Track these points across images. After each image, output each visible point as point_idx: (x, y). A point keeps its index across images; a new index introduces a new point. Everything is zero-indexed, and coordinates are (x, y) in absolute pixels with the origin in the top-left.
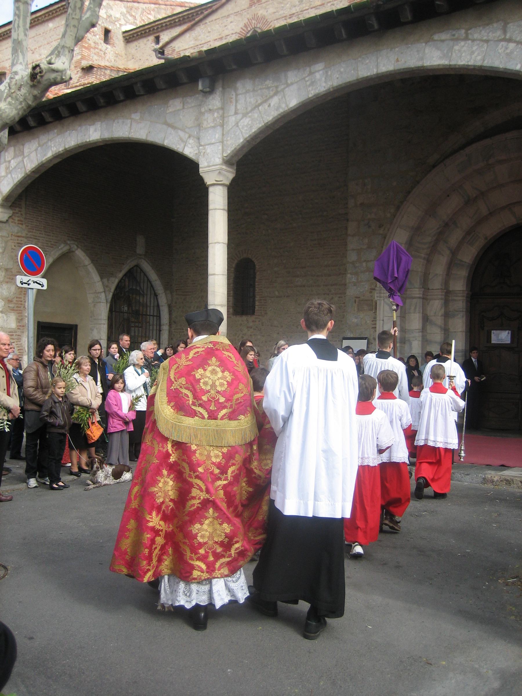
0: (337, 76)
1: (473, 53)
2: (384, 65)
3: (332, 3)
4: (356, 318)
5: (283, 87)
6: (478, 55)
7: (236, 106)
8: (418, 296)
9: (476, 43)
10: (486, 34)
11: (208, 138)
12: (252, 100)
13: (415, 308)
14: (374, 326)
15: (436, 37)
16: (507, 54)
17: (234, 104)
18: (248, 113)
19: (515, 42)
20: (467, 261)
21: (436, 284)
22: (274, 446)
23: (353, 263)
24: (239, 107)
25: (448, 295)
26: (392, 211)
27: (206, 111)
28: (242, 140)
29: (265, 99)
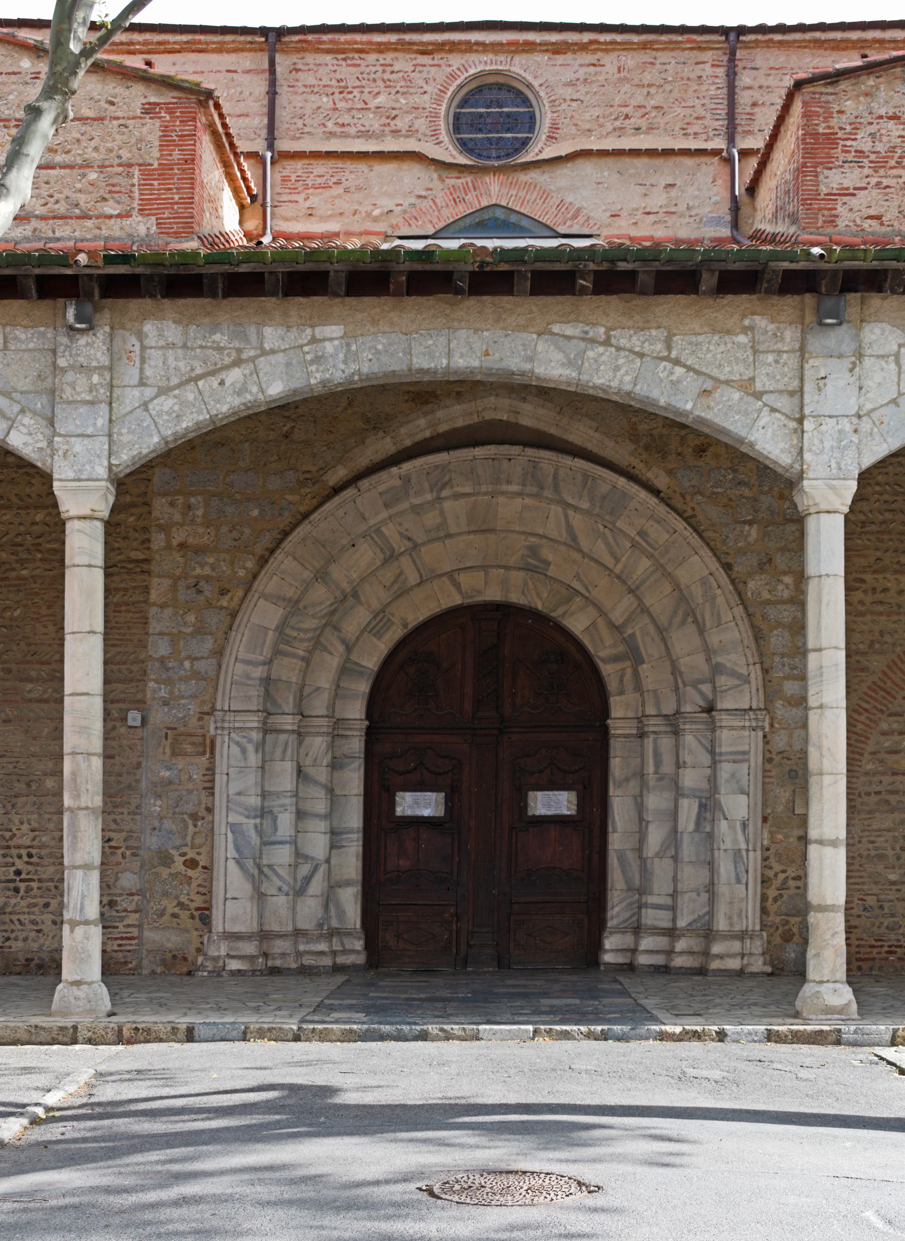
0: (370, 357)
1: (617, 368)
2: (462, 356)
3: (121, 121)
4: (168, 768)
5: (252, 353)
6: (627, 373)
7: (142, 370)
8: (289, 727)
9: (622, 353)
10: (639, 343)
11: (78, 422)
12: (181, 364)
13: (284, 752)
14: (208, 785)
15: (556, 328)
17: (138, 364)
18: (171, 389)
19: (684, 366)
20: (370, 666)
23: (162, 660)
24: (148, 372)
25: (337, 729)
26: (249, 565)
27: (72, 367)
29: (212, 368)
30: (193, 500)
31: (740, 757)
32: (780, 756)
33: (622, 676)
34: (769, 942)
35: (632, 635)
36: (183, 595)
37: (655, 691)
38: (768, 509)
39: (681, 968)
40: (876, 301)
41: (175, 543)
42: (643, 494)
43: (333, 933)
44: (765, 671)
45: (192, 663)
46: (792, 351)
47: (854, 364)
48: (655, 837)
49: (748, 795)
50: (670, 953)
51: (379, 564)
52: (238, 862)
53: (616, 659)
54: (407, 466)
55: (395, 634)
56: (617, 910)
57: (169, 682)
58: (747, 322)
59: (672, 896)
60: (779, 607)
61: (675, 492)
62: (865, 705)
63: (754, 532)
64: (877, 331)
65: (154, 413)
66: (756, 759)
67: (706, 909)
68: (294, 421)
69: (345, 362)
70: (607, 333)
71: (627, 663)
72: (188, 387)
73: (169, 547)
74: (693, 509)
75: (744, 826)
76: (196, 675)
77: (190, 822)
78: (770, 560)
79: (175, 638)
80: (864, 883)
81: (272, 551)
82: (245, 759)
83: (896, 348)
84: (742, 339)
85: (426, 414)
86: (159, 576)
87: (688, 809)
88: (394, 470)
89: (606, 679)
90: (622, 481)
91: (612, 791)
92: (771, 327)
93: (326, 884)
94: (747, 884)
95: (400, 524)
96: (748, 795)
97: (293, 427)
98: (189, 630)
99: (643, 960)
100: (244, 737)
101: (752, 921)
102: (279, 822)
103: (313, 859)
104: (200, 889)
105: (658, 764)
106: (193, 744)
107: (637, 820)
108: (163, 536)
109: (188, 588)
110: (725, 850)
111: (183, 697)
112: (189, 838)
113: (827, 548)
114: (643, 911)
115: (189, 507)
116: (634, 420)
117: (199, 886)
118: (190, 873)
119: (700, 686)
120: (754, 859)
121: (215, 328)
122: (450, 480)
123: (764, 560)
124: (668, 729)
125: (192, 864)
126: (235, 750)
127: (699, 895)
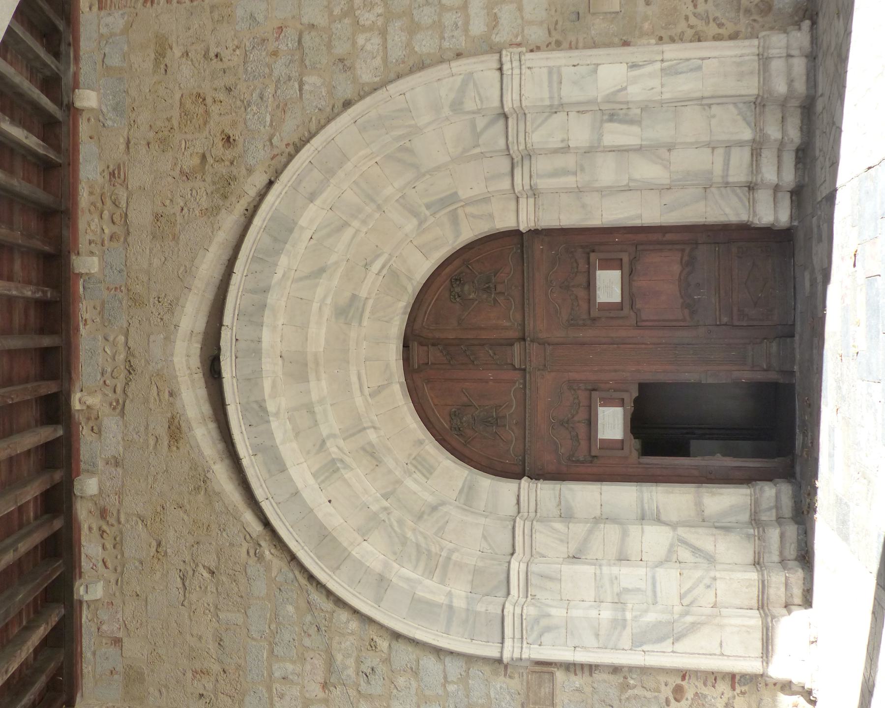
30: (277, 674)
31: (555, 77)
32: (553, 33)
33: (474, 216)
34: (772, 29)
35: (428, 206)
36: (377, 687)
38: (287, 66)
39: (801, 129)
41: (321, 695)
42: (270, 198)
43: (755, 521)
44: (459, 55)
45: (449, 683)
48: (647, 170)
49: (598, 65)
52: (677, 639)
53: (454, 219)
54: (243, 450)
59: (713, 148)
60: (389, 46)
61: (269, 166)
63: (311, 80)
66: (558, 58)
67: (731, 107)
68: (197, 565)
71: (460, 212)
74: (287, 145)
75: (633, 66)
77: (630, 692)
78: (341, 60)
85: (190, 429)
87: (617, 135)
90: (257, 221)
93: (700, 530)
94: (703, 59)
96: (598, 65)
97: (204, 567)
98: (414, 684)
99: (789, 177)
100: (532, 628)
101: (746, 49)
102: (630, 587)
103: (672, 545)
109: (368, 682)
110: (662, 86)
111: (488, 695)
112: (648, 694)
116: (197, 212)
117: (705, 684)
118: (690, 694)
119: (478, 130)
120: (672, 52)
123: (341, 66)
124: (526, 163)
127: (714, 116)
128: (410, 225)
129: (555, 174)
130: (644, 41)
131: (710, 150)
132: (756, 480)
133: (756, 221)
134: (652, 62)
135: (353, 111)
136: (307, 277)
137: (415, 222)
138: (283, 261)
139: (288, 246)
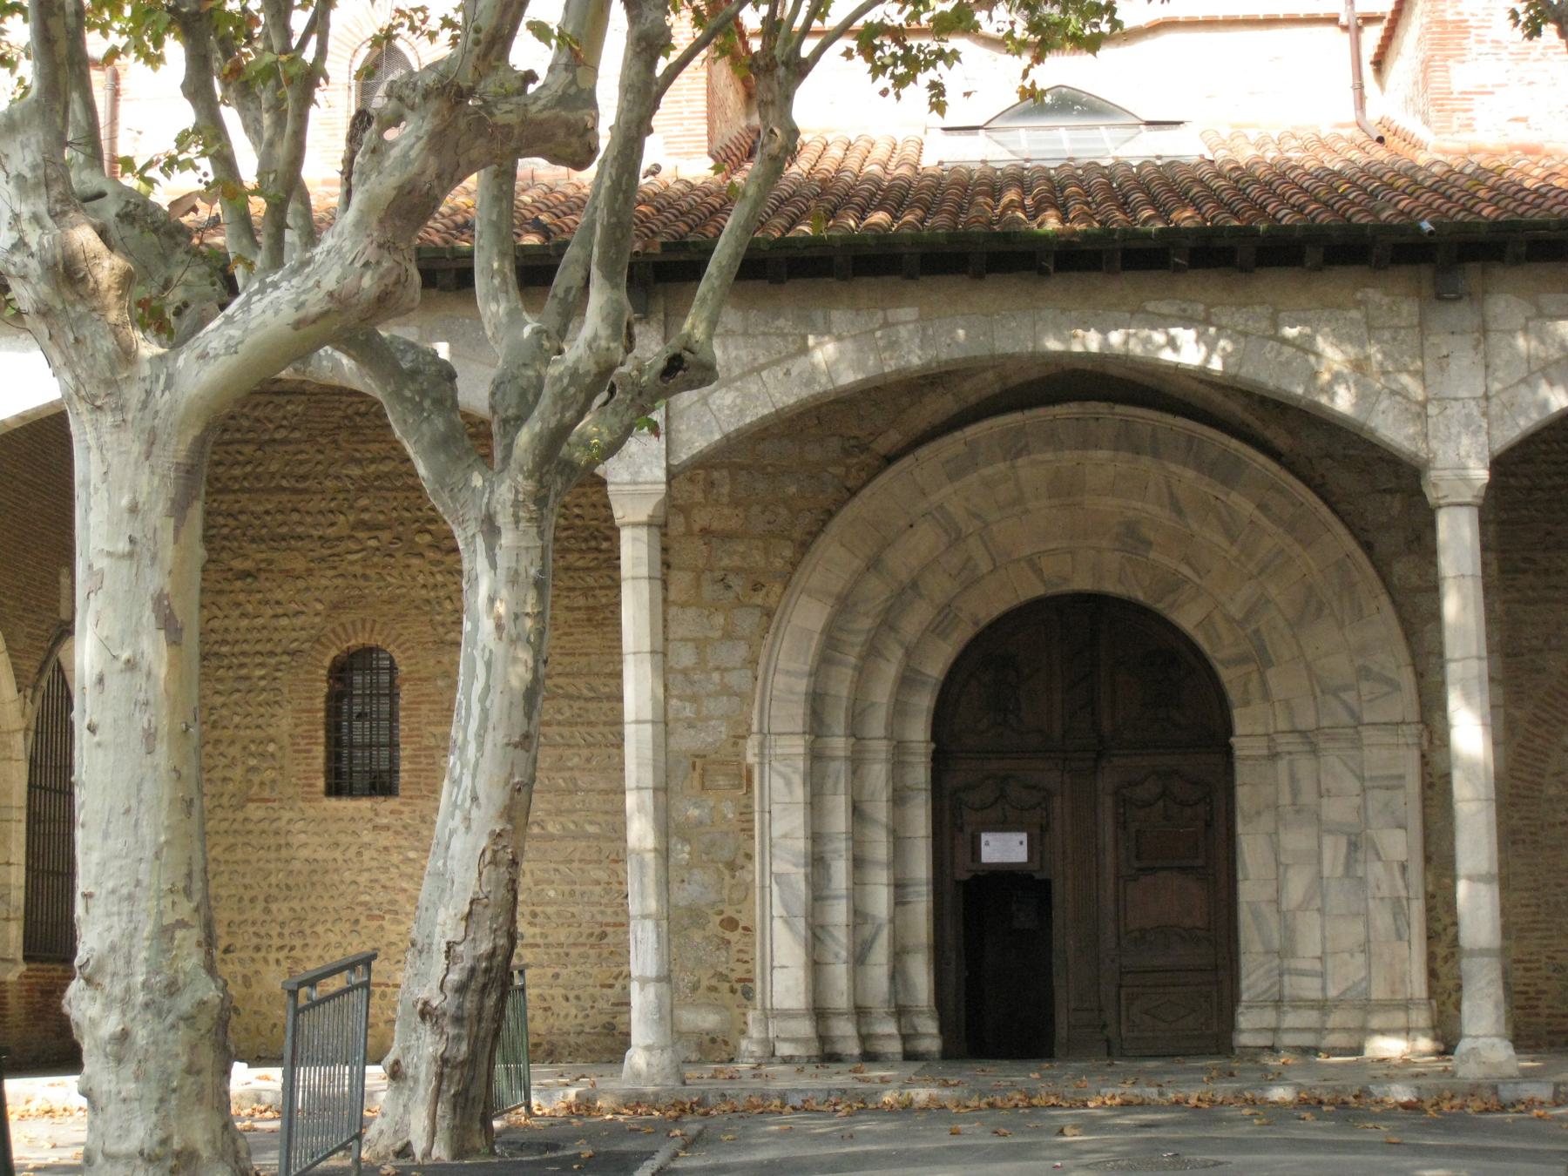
14: (745, 825)
15: (1151, 306)
16: (1280, 363)
21: (877, 725)
22: (1507, 987)
23: (685, 672)
26: (788, 553)
28: (717, 437)
30: (716, 475)
35: (1257, 631)
36: (708, 591)
37: (1287, 702)
40: (1498, 271)
41: (696, 528)
42: (1262, 459)
46: (1412, 327)
47: (1478, 340)
50: (1321, 1031)
51: (943, 548)
52: (786, 922)
53: (1242, 659)
54: (971, 431)
55: (962, 634)
56: (1254, 977)
57: (694, 699)
58: (1359, 295)
59: (1320, 958)
62: (1543, 715)
64: (1502, 304)
65: (714, 407)
67: (1363, 974)
69: (921, 348)
70: (1207, 311)
71: (1252, 667)
72: (751, 379)
73: (689, 533)
74: (1323, 476)
75: (1404, 868)
76: (727, 690)
77: (727, 873)
78: (1418, 538)
79: (701, 645)
80: (1552, 937)
81: (814, 535)
82: (791, 792)
83: (1523, 321)
84: (1355, 314)
86: (680, 569)
88: (958, 434)
89: (1227, 686)
90: (1234, 443)
91: (1240, 828)
92: (1386, 300)
95: (967, 499)
104: (741, 956)
105: (1295, 792)
106: (726, 775)
107: (1273, 864)
108: (682, 519)
110: (1382, 899)
111: (711, 718)
112: (726, 892)
113: (1458, 540)
114: (1286, 978)
115: (712, 484)
118: (728, 935)
121: (776, 316)
122: (1027, 445)
124: (1307, 748)
125: (731, 924)
126: (777, 782)
127: (1352, 956)
128: (1235, 610)
129: (1293, 779)
130: (1430, 878)
131: (1319, 953)
132: (941, 1015)
133: (1240, 1010)
134: (1407, 887)
135: (1360, 555)
136: (1171, 494)
137: (1239, 616)
138: (1190, 474)
139: (1207, 479)
